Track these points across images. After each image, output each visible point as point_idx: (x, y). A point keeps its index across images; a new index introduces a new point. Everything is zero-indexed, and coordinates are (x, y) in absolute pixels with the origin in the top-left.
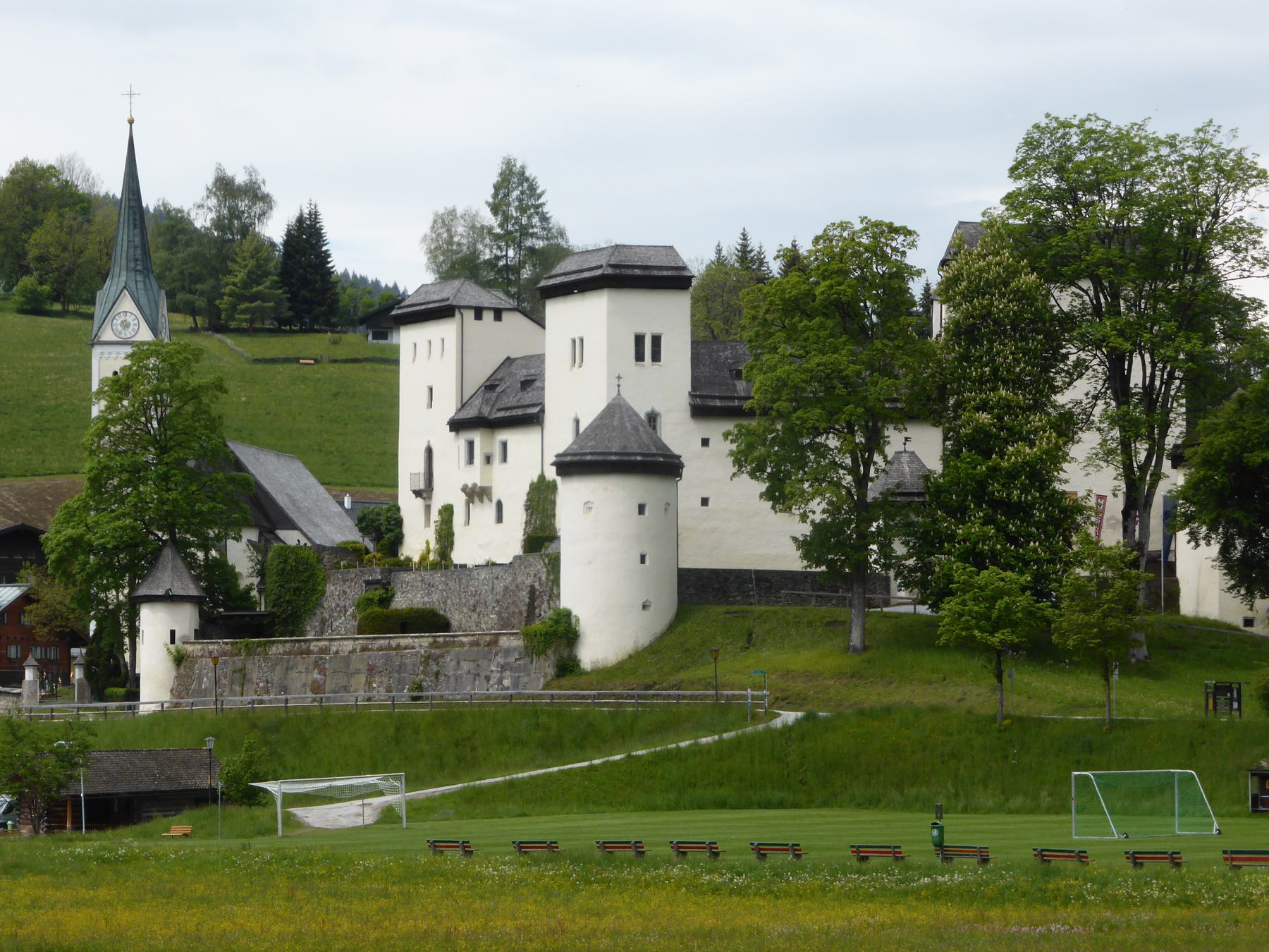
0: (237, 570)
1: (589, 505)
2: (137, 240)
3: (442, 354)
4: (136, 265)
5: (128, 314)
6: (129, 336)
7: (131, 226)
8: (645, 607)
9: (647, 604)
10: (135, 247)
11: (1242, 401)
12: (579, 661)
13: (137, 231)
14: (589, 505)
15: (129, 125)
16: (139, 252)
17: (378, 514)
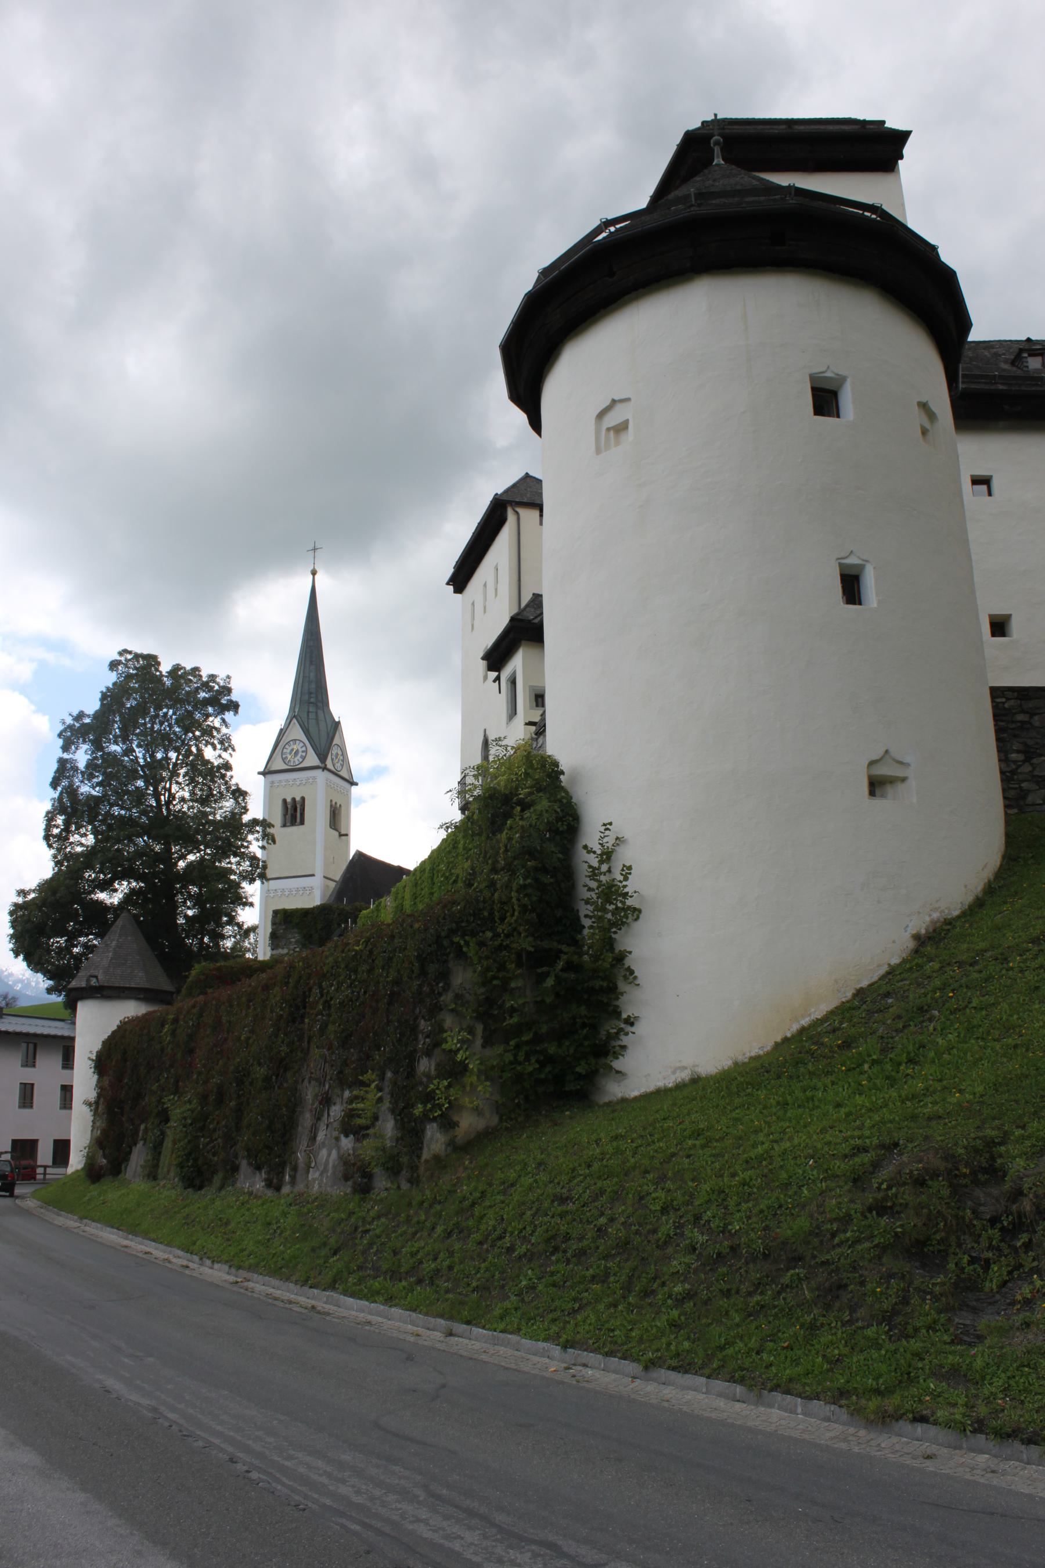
0: (11, 931)
1: (613, 419)
2: (312, 675)
3: (496, 595)
4: (310, 698)
5: (298, 742)
6: (297, 763)
7: (308, 663)
8: (876, 786)
9: (882, 770)
10: (310, 682)
11: (595, 1225)
12: (736, 1064)
13: (313, 668)
14: (613, 419)
15: (311, 576)
16: (313, 686)
17: (466, 878)
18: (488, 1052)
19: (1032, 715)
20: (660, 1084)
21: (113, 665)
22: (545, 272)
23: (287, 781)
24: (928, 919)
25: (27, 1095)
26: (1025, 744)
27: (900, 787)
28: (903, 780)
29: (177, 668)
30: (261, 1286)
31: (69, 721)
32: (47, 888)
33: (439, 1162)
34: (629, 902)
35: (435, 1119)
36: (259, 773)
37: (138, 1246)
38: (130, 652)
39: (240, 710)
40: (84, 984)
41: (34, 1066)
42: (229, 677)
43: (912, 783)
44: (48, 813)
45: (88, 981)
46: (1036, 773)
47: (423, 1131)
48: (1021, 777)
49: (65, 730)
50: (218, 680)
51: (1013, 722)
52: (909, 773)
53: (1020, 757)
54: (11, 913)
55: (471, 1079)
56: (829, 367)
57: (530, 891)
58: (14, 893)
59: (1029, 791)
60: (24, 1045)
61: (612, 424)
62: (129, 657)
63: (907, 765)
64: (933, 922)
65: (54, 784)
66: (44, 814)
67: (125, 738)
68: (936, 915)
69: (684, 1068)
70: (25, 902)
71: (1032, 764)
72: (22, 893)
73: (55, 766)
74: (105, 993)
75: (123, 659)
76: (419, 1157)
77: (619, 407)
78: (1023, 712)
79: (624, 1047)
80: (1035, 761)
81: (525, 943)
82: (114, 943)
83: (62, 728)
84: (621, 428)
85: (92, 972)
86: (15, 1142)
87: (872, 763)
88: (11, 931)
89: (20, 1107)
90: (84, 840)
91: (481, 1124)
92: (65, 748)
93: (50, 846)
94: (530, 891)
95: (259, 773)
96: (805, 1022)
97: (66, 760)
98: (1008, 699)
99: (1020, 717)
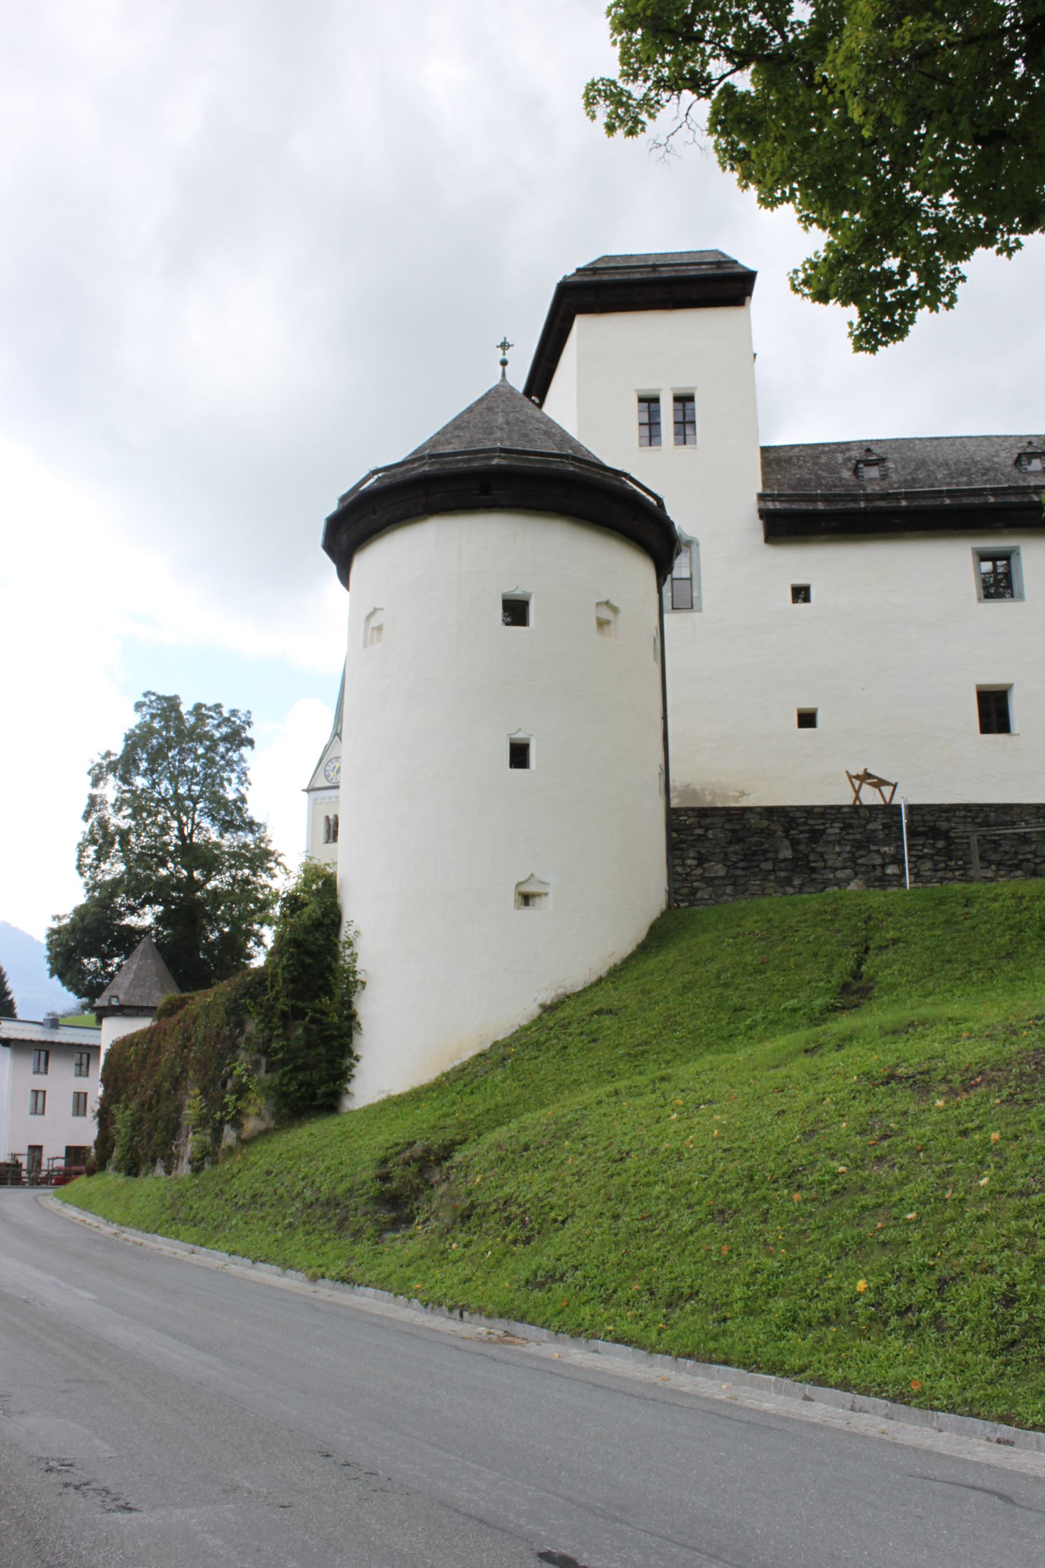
8: (527, 899)
9: (527, 889)
14: (375, 622)
18: (269, 1076)
19: (707, 829)
20: (371, 1102)
21: (139, 706)
22: (342, 499)
23: (330, 798)
24: (553, 993)
25: (38, 1101)
26: (699, 852)
27: (544, 899)
28: (546, 894)
29: (198, 707)
30: (133, 1236)
31: (98, 760)
32: (80, 912)
33: (230, 1150)
34: (358, 977)
35: (228, 1121)
36: (303, 790)
37: (90, 1219)
38: (154, 694)
39: (256, 745)
40: (106, 1004)
41: (87, 1075)
42: (249, 712)
43: (551, 897)
44: (80, 844)
45: (110, 1001)
46: (706, 875)
47: (223, 1130)
48: (693, 878)
49: (93, 769)
50: (240, 714)
51: (692, 835)
52: (549, 890)
53: (694, 862)
54: (49, 936)
55: (251, 1096)
56: (516, 589)
57: (292, 968)
58: (51, 919)
59: (698, 889)
60: (78, 1055)
61: (375, 625)
62: (153, 698)
63: (548, 884)
64: (558, 996)
65: (86, 816)
66: (76, 845)
67: (151, 771)
68: (560, 991)
69: (383, 1091)
70: (60, 927)
71: (703, 869)
72: (57, 918)
73: (87, 801)
74: (125, 1011)
75: (147, 700)
76: (219, 1147)
77: (379, 613)
78: (701, 827)
79: (353, 1076)
80: (705, 865)
81: (281, 1005)
82: (135, 967)
83: (91, 766)
84: (380, 629)
85: (115, 992)
86: (69, 1149)
87: (519, 884)
88: (48, 953)
89: (73, 1115)
90: (114, 868)
91: (262, 1126)
92: (95, 784)
93: (82, 874)
94: (292, 968)
95: (303, 790)
96: (457, 1063)
97: (96, 796)
98: (689, 817)
99: (698, 831)
